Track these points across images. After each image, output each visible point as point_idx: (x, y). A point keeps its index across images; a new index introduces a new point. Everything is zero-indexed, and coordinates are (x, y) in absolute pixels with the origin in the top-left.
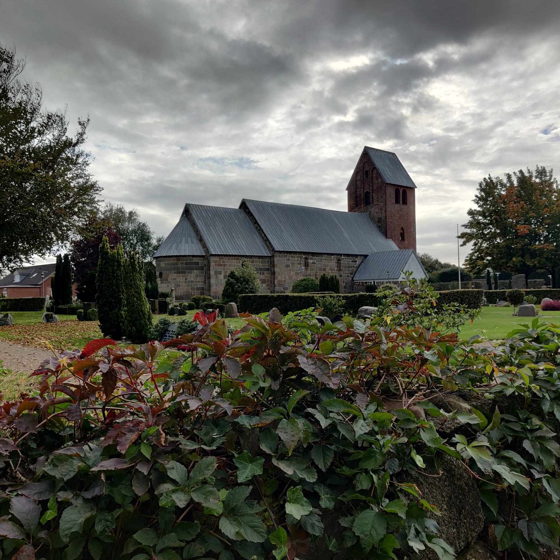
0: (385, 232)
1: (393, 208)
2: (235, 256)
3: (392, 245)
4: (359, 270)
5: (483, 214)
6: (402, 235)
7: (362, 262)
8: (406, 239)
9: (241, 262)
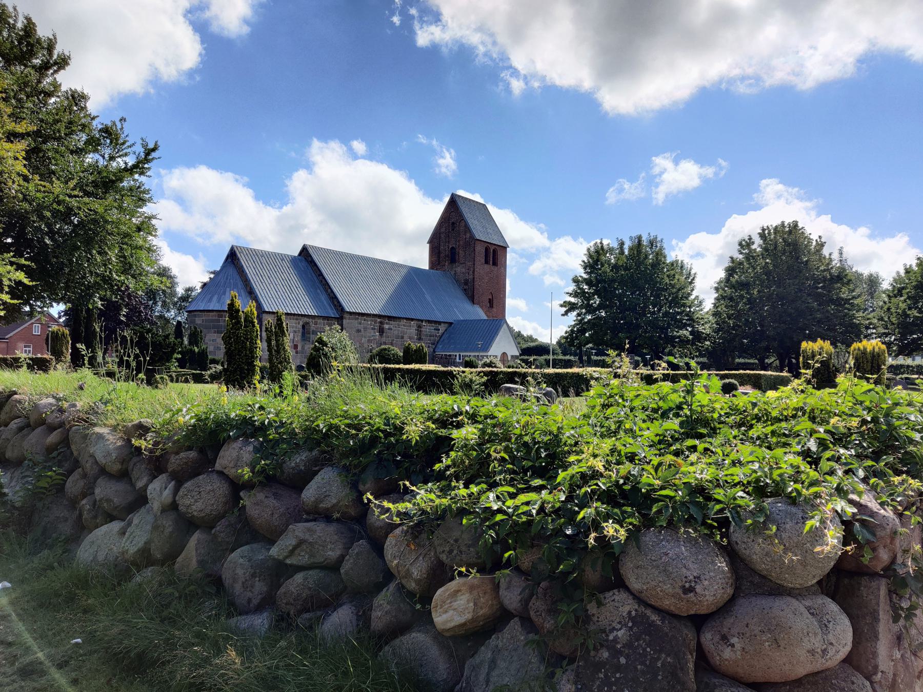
0: (472, 298)
1: (482, 269)
2: (294, 315)
3: (479, 313)
4: (442, 339)
5: (588, 282)
6: (491, 302)
7: (446, 330)
8: (494, 306)
9: (301, 323)
